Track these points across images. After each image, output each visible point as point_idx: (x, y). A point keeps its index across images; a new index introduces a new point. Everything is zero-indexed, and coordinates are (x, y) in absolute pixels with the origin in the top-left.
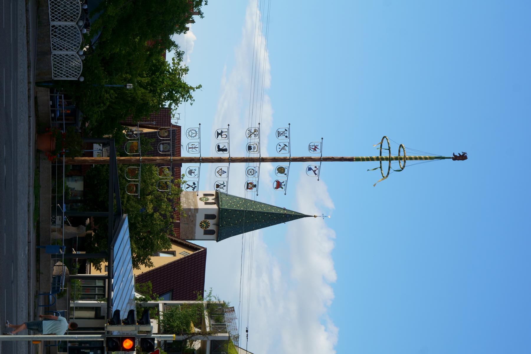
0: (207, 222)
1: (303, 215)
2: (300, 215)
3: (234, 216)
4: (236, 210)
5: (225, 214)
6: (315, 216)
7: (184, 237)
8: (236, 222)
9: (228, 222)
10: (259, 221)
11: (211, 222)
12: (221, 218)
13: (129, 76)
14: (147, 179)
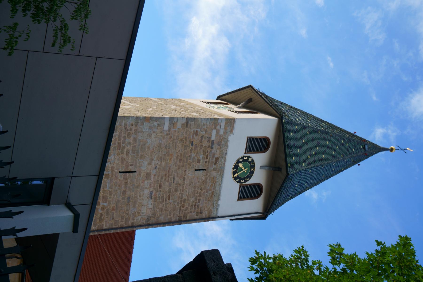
6: (392, 150)
7: (193, 213)
8: (309, 157)
13: (331, 272)
14: (358, 140)
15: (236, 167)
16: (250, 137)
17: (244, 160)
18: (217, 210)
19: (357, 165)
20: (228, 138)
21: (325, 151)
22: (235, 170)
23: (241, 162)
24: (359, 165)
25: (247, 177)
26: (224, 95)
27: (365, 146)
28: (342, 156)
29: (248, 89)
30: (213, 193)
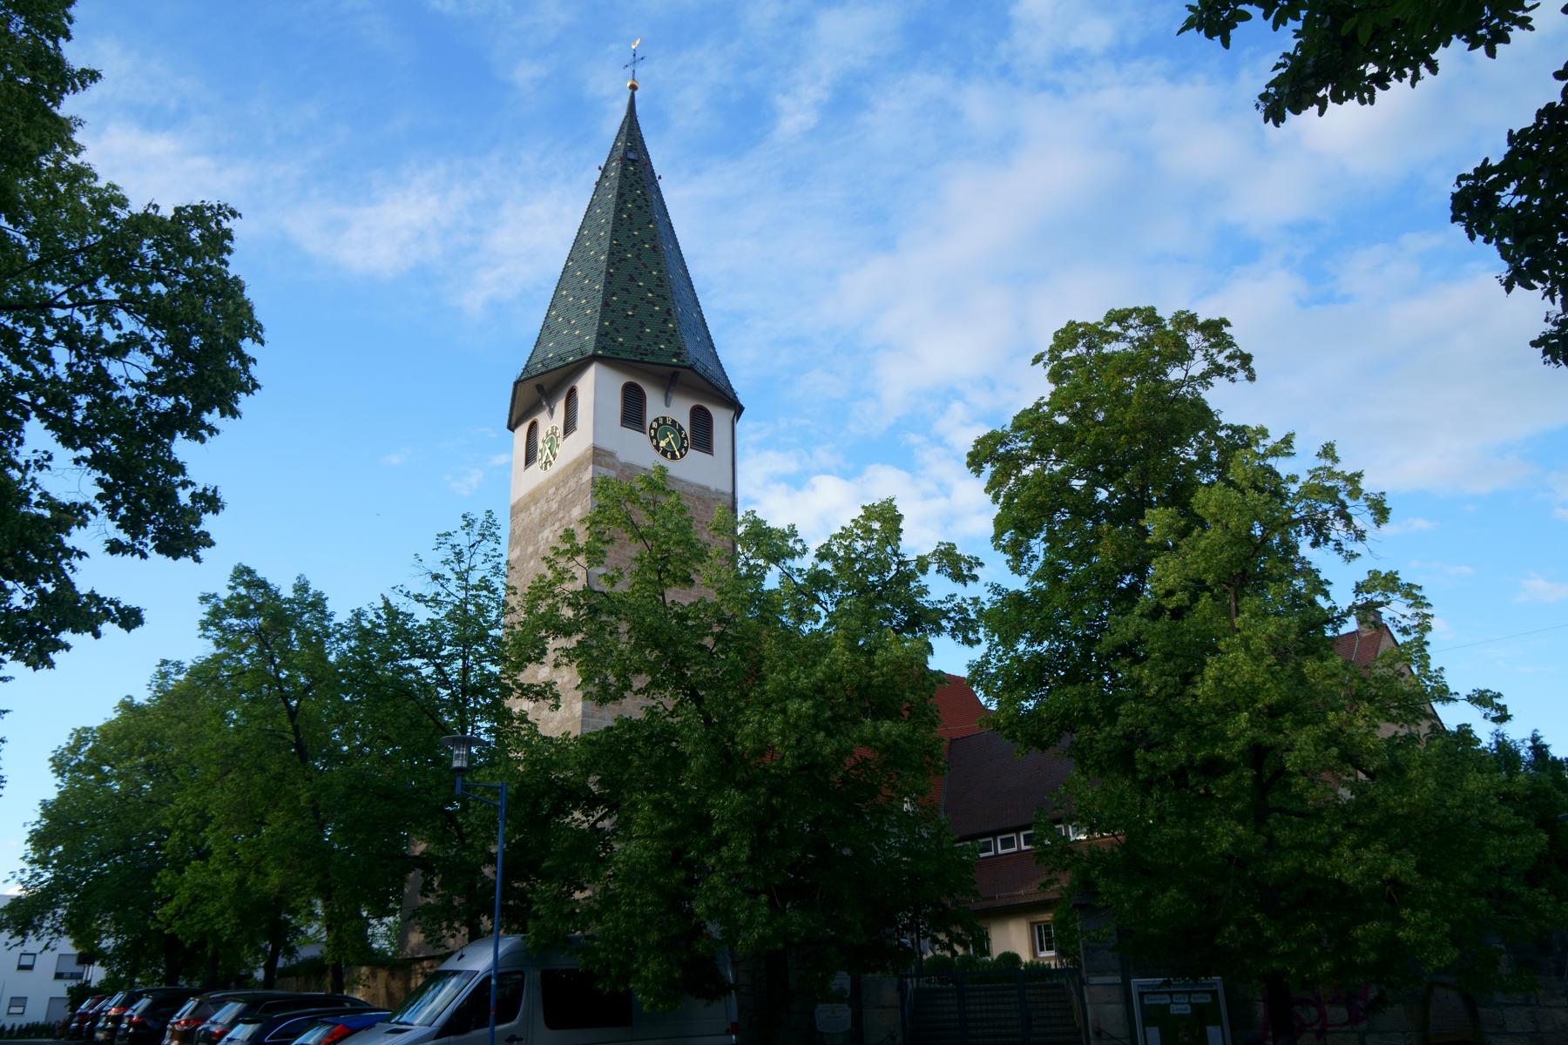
0: (655, 425)
1: (628, 120)
2: (625, 130)
3: (630, 313)
4: (606, 304)
5: (621, 340)
6: (633, 88)
8: (657, 308)
9: (657, 336)
10: (652, 240)
11: (656, 406)
12: (641, 354)
15: (664, 453)
16: (622, 422)
17: (655, 437)
18: (723, 493)
19: (660, 182)
20: (621, 463)
21: (646, 267)
22: (669, 455)
23: (658, 443)
24: (660, 177)
25: (681, 434)
26: (510, 421)
27: (629, 159)
28: (651, 226)
29: (519, 388)
30: (699, 498)
